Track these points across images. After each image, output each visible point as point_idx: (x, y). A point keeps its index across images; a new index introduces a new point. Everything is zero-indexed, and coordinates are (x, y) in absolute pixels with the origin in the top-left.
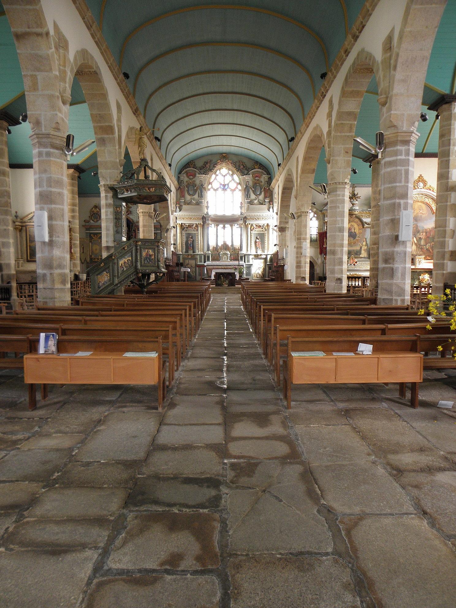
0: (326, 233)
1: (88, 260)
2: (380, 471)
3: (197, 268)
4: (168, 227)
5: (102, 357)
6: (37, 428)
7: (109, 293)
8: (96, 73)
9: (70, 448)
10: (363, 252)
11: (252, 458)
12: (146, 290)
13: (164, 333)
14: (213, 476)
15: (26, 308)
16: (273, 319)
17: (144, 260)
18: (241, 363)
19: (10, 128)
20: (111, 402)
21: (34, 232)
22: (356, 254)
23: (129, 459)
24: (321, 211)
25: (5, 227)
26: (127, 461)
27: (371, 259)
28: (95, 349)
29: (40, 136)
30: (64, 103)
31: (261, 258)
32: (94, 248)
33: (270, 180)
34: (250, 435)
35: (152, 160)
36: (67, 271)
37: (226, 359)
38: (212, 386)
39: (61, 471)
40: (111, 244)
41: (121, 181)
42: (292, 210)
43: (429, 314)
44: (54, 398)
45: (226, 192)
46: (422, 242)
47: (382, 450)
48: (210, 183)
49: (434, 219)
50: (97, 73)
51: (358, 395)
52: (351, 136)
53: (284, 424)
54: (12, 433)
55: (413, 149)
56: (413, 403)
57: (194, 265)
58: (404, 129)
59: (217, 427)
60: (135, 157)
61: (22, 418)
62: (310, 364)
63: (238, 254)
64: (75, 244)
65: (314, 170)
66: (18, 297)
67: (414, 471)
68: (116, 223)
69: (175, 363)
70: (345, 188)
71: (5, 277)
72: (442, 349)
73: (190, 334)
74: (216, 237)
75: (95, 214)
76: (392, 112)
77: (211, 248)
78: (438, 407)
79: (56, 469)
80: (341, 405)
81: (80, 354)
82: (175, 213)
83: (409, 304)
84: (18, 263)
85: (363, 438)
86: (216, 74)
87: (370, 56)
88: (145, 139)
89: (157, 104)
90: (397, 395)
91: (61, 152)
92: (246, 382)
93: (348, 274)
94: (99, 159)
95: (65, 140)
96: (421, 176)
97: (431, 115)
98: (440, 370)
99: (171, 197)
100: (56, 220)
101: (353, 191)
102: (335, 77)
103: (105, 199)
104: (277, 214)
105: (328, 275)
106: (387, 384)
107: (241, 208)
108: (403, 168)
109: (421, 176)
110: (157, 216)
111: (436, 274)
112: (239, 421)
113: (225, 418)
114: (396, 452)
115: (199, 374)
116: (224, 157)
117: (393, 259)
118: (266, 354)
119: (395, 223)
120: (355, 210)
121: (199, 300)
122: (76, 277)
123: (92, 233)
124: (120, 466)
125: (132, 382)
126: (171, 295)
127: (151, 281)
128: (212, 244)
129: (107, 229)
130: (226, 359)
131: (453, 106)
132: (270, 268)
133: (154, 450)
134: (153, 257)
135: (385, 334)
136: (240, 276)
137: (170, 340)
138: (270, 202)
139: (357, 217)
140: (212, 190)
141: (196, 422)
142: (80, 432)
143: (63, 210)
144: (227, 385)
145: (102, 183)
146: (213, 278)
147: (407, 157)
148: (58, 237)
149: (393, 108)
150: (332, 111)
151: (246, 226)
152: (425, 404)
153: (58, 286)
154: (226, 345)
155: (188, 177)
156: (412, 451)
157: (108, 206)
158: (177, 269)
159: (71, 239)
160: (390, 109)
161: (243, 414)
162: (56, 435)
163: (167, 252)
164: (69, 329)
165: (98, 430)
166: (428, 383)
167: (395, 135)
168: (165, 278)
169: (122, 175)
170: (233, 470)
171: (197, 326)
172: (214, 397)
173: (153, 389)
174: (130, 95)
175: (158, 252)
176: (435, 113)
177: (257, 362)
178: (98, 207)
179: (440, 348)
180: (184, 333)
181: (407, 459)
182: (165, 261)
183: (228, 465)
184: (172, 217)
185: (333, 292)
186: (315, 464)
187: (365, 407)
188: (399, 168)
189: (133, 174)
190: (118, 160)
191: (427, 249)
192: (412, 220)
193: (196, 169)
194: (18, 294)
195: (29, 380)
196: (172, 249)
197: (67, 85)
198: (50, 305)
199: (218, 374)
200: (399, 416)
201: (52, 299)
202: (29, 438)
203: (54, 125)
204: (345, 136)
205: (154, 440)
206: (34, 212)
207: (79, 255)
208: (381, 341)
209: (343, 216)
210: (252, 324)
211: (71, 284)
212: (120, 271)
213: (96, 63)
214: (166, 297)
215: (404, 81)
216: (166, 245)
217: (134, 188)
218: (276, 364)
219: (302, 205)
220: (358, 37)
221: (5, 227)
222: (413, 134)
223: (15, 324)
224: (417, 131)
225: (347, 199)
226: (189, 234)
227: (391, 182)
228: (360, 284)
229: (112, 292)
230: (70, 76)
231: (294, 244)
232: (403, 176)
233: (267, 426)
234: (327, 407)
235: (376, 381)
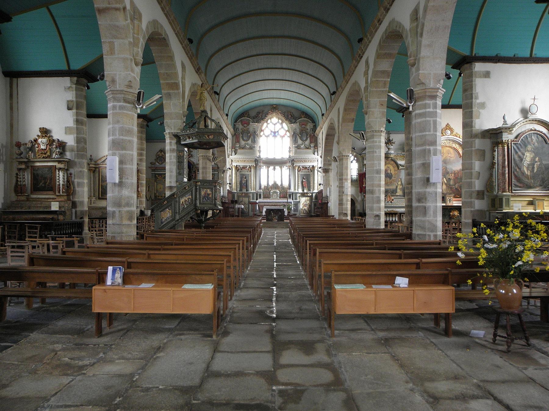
0: (365, 174)
1: (153, 197)
2: (418, 398)
3: (250, 205)
4: (224, 169)
5: (164, 289)
6: (101, 355)
7: (171, 228)
8: (164, 39)
9: (131, 374)
10: (398, 190)
11: (298, 385)
12: (204, 225)
13: (219, 266)
14: (262, 402)
15: (96, 241)
16: (318, 253)
17: (203, 199)
18: (289, 293)
19: (89, 84)
20: (170, 330)
21: (106, 173)
22: (393, 192)
23: (185, 385)
24: (360, 155)
25: (80, 169)
26: (183, 387)
27: (406, 197)
28: (157, 281)
29: (115, 92)
30: (136, 65)
31: (308, 196)
32: (159, 188)
33: (315, 128)
34: (297, 362)
35: (211, 111)
36: (134, 209)
37: (275, 290)
38: (263, 316)
39: (123, 396)
40: (174, 184)
41: (184, 129)
42: (335, 154)
43: (458, 249)
44: (118, 326)
45: (276, 138)
46: (452, 182)
47: (419, 378)
48: (262, 131)
49: (461, 162)
50: (165, 39)
51: (397, 325)
52: (385, 91)
53: (328, 352)
54: (79, 359)
55: (439, 103)
56: (447, 332)
57: (247, 202)
58: (431, 86)
59: (266, 355)
60: (197, 109)
61: (88, 345)
62: (352, 296)
63: (287, 192)
64: (142, 183)
65: (353, 119)
66: (89, 231)
67: (450, 399)
68: (179, 166)
69: (229, 294)
70: (381, 135)
71: (78, 213)
72: (471, 283)
73: (243, 266)
74: (268, 177)
75: (161, 158)
76: (420, 72)
77: (262, 187)
78: (470, 337)
79: (118, 394)
80: (381, 334)
81: (144, 286)
82: (231, 157)
83: (441, 239)
84: (91, 200)
85: (402, 366)
86: (268, 39)
87: (400, 25)
88: (206, 94)
89: (216, 64)
90: (432, 325)
91: (133, 106)
92: (294, 311)
93: (386, 210)
94: (165, 111)
95: (136, 96)
96: (448, 125)
97: (455, 73)
98: (471, 301)
99: (228, 144)
100: (125, 164)
101: (389, 138)
102: (370, 42)
103: (169, 145)
104: (321, 157)
105: (368, 212)
106: (422, 314)
107: (290, 152)
108: (432, 119)
109: (448, 124)
110: (214, 159)
111: (465, 211)
112: (287, 349)
113: (274, 346)
114: (432, 380)
115: (251, 303)
116: (275, 108)
117: (426, 199)
118: (311, 285)
119: (426, 167)
120: (390, 154)
121: (251, 234)
122: (142, 213)
123: (157, 174)
124: (176, 391)
125: (189, 312)
126: (227, 230)
127: (209, 217)
128: (264, 183)
129: (171, 171)
130: (275, 290)
131: (473, 66)
132: (315, 205)
133: (208, 376)
134: (211, 196)
135: (419, 269)
136: (289, 212)
137: (225, 273)
138: (314, 146)
139: (392, 160)
140: (263, 136)
141: (247, 350)
142: (142, 359)
143: (132, 155)
144: (276, 315)
145: (167, 131)
146: (264, 213)
147: (435, 110)
148: (128, 179)
149: (421, 68)
150: (368, 70)
151: (294, 168)
152: (458, 334)
153: (126, 222)
154: (275, 276)
155: (243, 125)
156: (447, 379)
157: (172, 151)
158: (232, 205)
159: (138, 179)
160: (418, 69)
161: (291, 343)
162: (119, 361)
163: (223, 191)
164: (132, 262)
165: (157, 357)
166: (461, 313)
167: (423, 91)
168: (221, 214)
169: (184, 124)
170: (280, 396)
171: (250, 258)
172: (264, 326)
173: (207, 318)
174: (193, 57)
175: (216, 191)
176: (458, 71)
177: (304, 292)
178: (163, 151)
179: (470, 282)
180: (237, 266)
181: (442, 387)
182: (222, 199)
183: (277, 392)
184: (228, 160)
185: (372, 227)
186: (357, 391)
187: (403, 336)
188: (428, 119)
189: (194, 123)
190: (182, 112)
191: (456, 189)
192: (441, 164)
193: (248, 121)
194: (89, 228)
195: (96, 309)
196: (228, 188)
197: (139, 50)
198: (118, 239)
199: (268, 304)
200: (435, 344)
201: (119, 233)
202: (94, 364)
203: (127, 83)
204: (380, 91)
205: (208, 367)
206: (107, 156)
207: (145, 193)
208: (416, 275)
209: (380, 160)
210: (299, 256)
211: (137, 219)
212: (181, 209)
213: (165, 32)
214: (222, 231)
215: (429, 46)
216: (223, 184)
217: (195, 136)
218: (321, 295)
219: (344, 150)
220: (389, 9)
221: (80, 169)
222: (439, 90)
223: (86, 257)
224: (442, 87)
225: (383, 144)
226: (243, 175)
227: (421, 131)
228: (397, 219)
229: (173, 227)
230: (142, 42)
231: (337, 183)
232: (432, 125)
233: (312, 354)
234: (368, 336)
235: (412, 312)
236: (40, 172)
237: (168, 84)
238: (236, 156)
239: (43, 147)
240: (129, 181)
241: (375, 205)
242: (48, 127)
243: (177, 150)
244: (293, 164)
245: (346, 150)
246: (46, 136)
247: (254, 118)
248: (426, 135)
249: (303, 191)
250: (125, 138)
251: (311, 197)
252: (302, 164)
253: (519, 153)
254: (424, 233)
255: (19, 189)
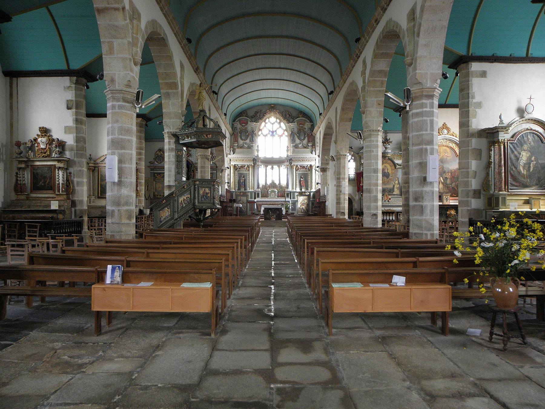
0: (362, 173)
1: (152, 196)
2: (415, 396)
3: (248, 204)
4: (223, 168)
5: (162, 287)
6: (101, 353)
7: (170, 227)
8: (163, 39)
9: (130, 372)
10: (395, 189)
11: (296, 383)
12: (202, 224)
13: (217, 265)
14: (260, 400)
15: (95, 239)
16: (315, 252)
17: (201, 198)
18: (286, 292)
19: (88, 84)
20: (169, 329)
21: (105, 172)
22: (390, 192)
23: (184, 383)
24: (358, 154)
25: (80, 169)
26: (182, 385)
27: (403, 196)
28: (156, 280)
29: (114, 92)
30: (135, 64)
31: (305, 195)
32: (157, 187)
33: (312, 127)
34: (295, 361)
35: (210, 110)
36: (133, 208)
37: (273, 288)
38: (261, 314)
39: (122, 394)
40: (172, 183)
41: (182, 129)
42: (332, 153)
43: (455, 248)
44: (117, 324)
45: (274, 137)
46: (448, 182)
47: (416, 376)
48: (260, 130)
49: (458, 161)
50: (164, 39)
51: (394, 323)
52: (383, 90)
53: (326, 351)
54: (79, 357)
55: (436, 102)
56: (444, 331)
57: (245, 201)
58: (428, 86)
59: (264, 353)
60: (196, 108)
61: (87, 343)
62: (350, 295)
63: (285, 191)
64: (141, 183)
65: (351, 118)
66: (89, 229)
67: (446, 397)
68: (177, 165)
69: (228, 292)
70: (378, 135)
71: (78, 212)
72: (468, 281)
73: (241, 264)
74: (266, 176)
75: (160, 157)
76: (417, 71)
77: (261, 186)
78: (467, 335)
79: (117, 392)
80: (378, 333)
81: (143, 284)
82: (229, 156)
83: (438, 238)
84: (90, 199)
85: (399, 364)
86: (266, 39)
87: (397, 24)
88: (204, 94)
89: (214, 63)
90: (428, 323)
91: (132, 105)
92: (292, 310)
93: (383, 209)
94: (164, 110)
95: (135, 95)
96: (444, 124)
97: (451, 73)
98: (467, 299)
99: (226, 143)
100: (125, 163)
101: (386, 137)
102: (367, 42)
103: (168, 144)
104: (319, 156)
105: (365, 211)
106: (419, 313)
107: (288, 151)
108: (428, 119)
109: (445, 123)
110: (213, 158)
111: (462, 210)
112: (285, 347)
113: (272, 344)
114: (429, 378)
115: (249, 302)
116: (273, 107)
117: (423, 198)
118: (309, 283)
119: (423, 166)
120: (387, 153)
121: (249, 232)
122: (141, 212)
123: (156, 173)
124: (175, 389)
125: (188, 311)
126: (225, 228)
127: (207, 215)
128: (262, 182)
129: (170, 171)
130: (273, 288)
131: (470, 66)
132: (313, 204)
133: (207, 374)
134: (209, 195)
135: (416, 267)
136: (287, 211)
137: (223, 271)
138: (312, 146)
139: (389, 159)
140: (262, 135)
141: (245, 348)
142: (141, 357)
143: (131, 154)
144: (274, 313)
145: (166, 130)
146: (262, 212)
147: (432, 110)
148: (127, 178)
149: (418, 68)
150: (365, 70)
151: (292, 167)
152: (455, 332)
153: (125, 221)
154: (273, 275)
155: (241, 124)
156: (444, 377)
157: (170, 150)
158: (230, 204)
159: (137, 178)
160: (415, 69)
161: (289, 341)
162: (118, 359)
163: (222, 190)
164: (131, 261)
165: (156, 355)
166: (457, 312)
167: (420, 90)
168: (220, 213)
169: (183, 123)
170: (278, 394)
171: (248, 257)
172: (262, 324)
173: (205, 317)
174: (191, 56)
175: (214, 191)
176: (455, 71)
177: (301, 291)
178: (162, 150)
179: (466, 280)
180: (236, 264)
181: (439, 385)
182: (220, 198)
183: (275, 390)
184: (226, 160)
185: (369, 226)
186: (354, 389)
187: (400, 334)
188: (425, 118)
189: (193, 123)
190: (180, 111)
191: (453, 188)
192: (437, 163)
193: (246, 120)
194: (88, 227)
195: (96, 308)
196: (226, 187)
197: (138, 50)
198: (117, 238)
199: (266, 302)
200: (431, 343)
201: (119, 232)
202: (93, 362)
203: (126, 83)
204: (377, 90)
205: (206, 365)
206: (106, 155)
207: (144, 192)
208: (412, 273)
209: (377, 159)
210: (297, 255)
211: (136, 218)
212: (180, 208)
213: (164, 32)
214: (220, 230)
215: (426, 45)
216: (221, 183)
217: (193, 135)
218: (319, 293)
219: (341, 149)
220: (386, 9)
221: (80, 169)
222: (436, 90)
223: (85, 256)
224: (439, 87)
225: (380, 144)
226: (241, 174)
227: (418, 131)
228: (394, 218)
229: (172, 226)
230: (141, 42)
231: (335, 182)
232: (429, 125)
233: (310, 352)
234: (366, 335)
235: (409, 311)
236: (39, 171)
237: (166, 84)
238: (234, 156)
239: (42, 146)
240: (128, 180)
241: (372, 204)
242: (47, 126)
243: (176, 149)
244: (291, 163)
245: (344, 150)
246: (45, 135)
247: (252, 118)
248: (423, 134)
249: (301, 190)
250: (124, 137)
251: (309, 196)
252: (299, 164)
253: (516, 152)
254: (421, 232)
255: (19, 188)
